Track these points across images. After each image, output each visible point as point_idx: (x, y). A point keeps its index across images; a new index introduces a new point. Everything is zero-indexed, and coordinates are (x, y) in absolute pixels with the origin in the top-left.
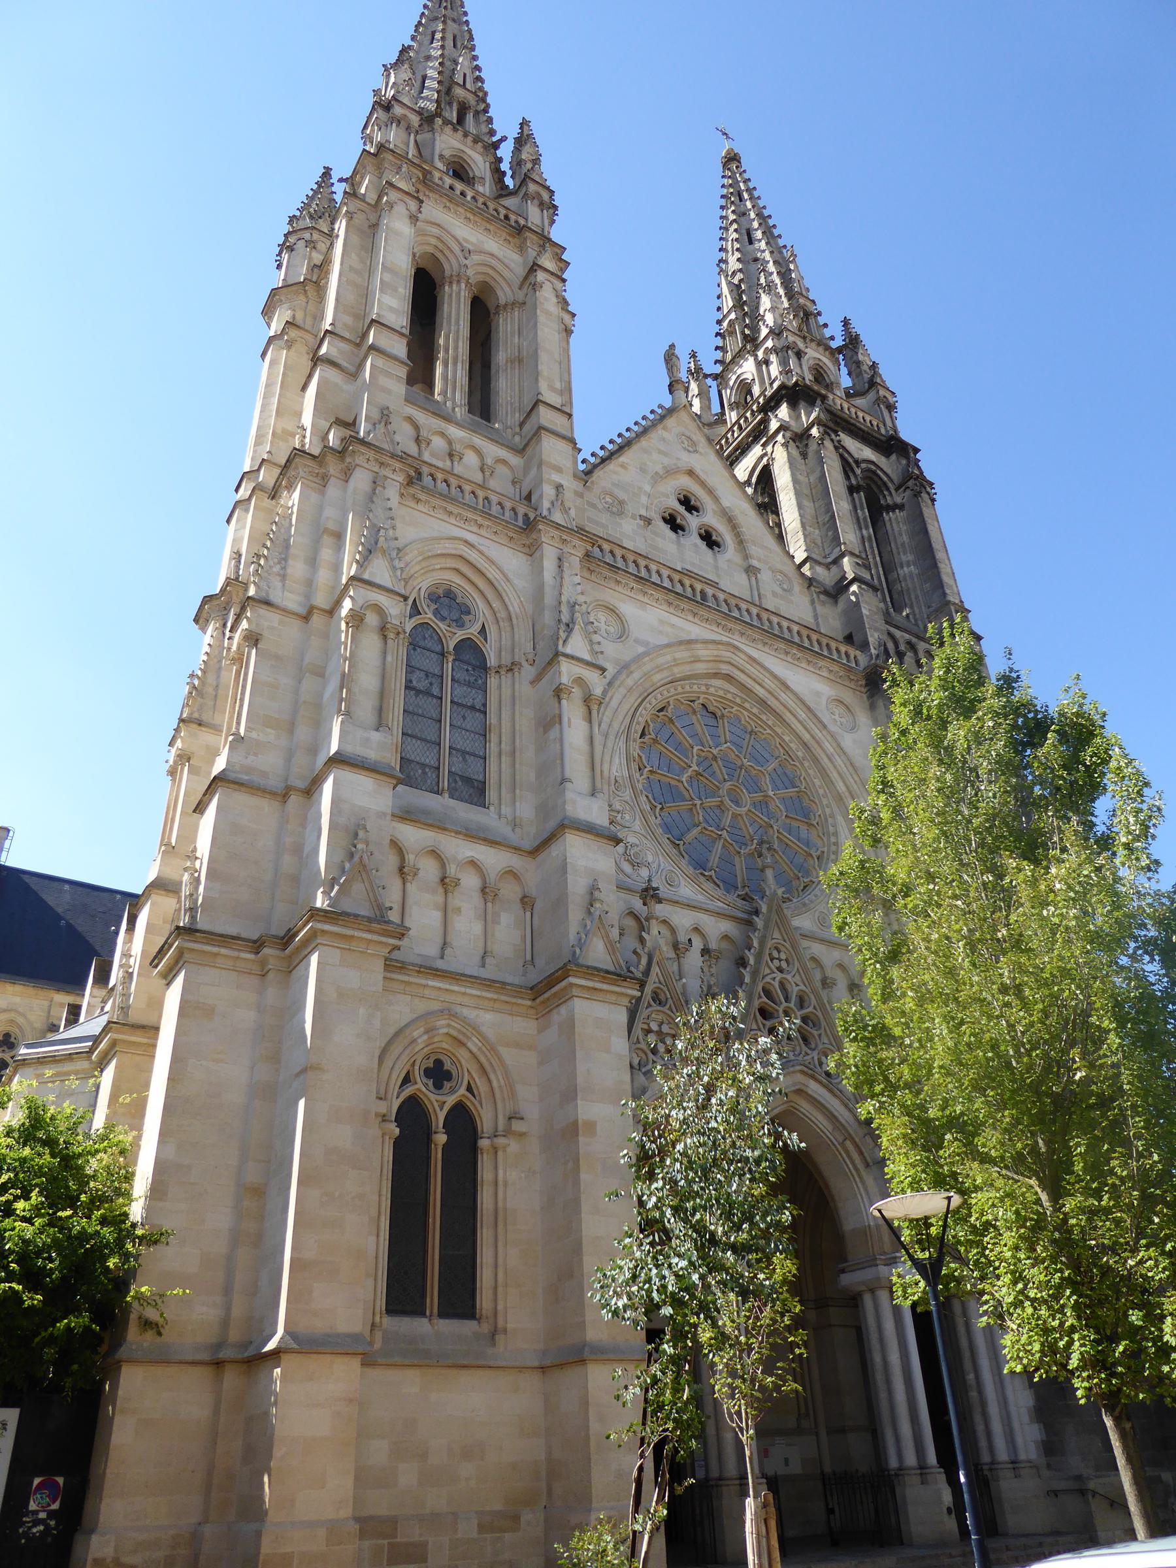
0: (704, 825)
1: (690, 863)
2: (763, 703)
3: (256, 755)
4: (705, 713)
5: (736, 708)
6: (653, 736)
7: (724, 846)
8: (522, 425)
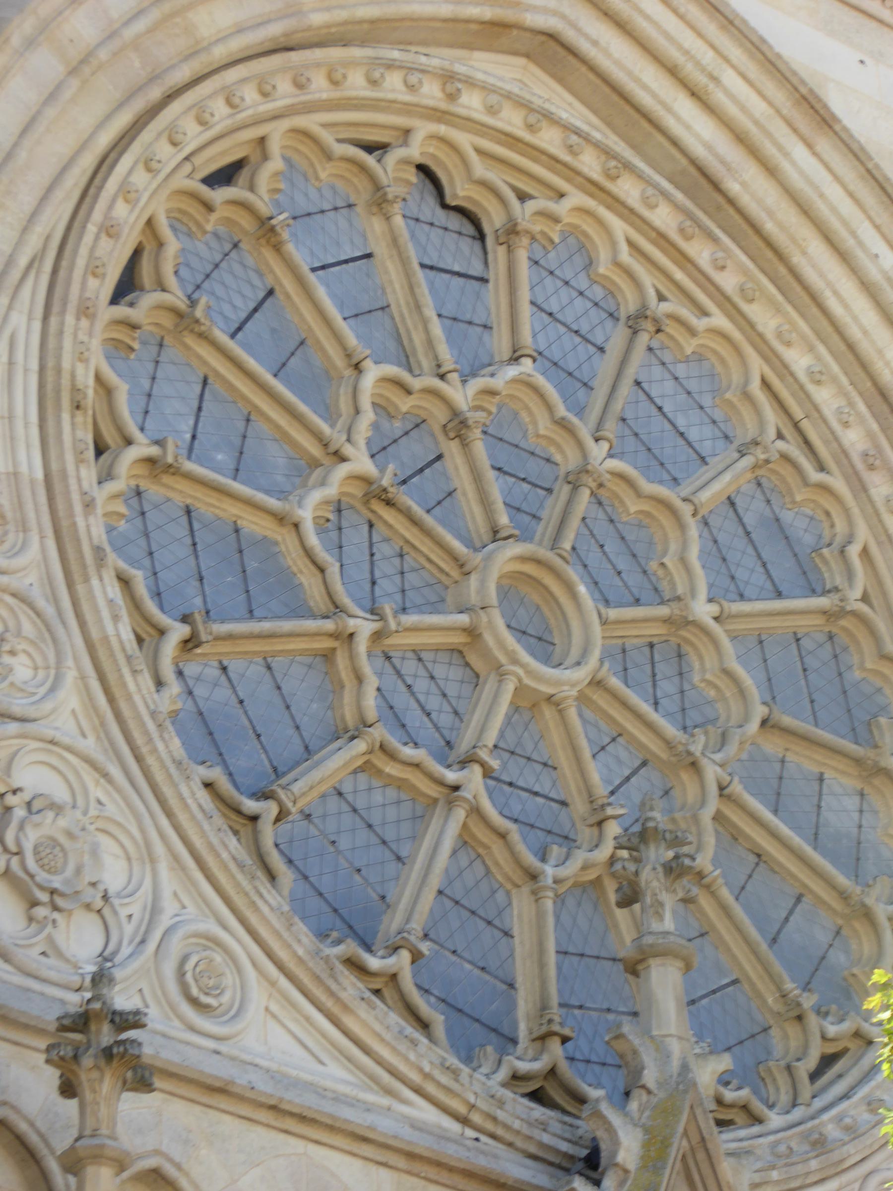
0: (379, 733)
1: (298, 906)
4: (430, 209)
5: (576, 198)
6: (176, 297)
7: (465, 841)
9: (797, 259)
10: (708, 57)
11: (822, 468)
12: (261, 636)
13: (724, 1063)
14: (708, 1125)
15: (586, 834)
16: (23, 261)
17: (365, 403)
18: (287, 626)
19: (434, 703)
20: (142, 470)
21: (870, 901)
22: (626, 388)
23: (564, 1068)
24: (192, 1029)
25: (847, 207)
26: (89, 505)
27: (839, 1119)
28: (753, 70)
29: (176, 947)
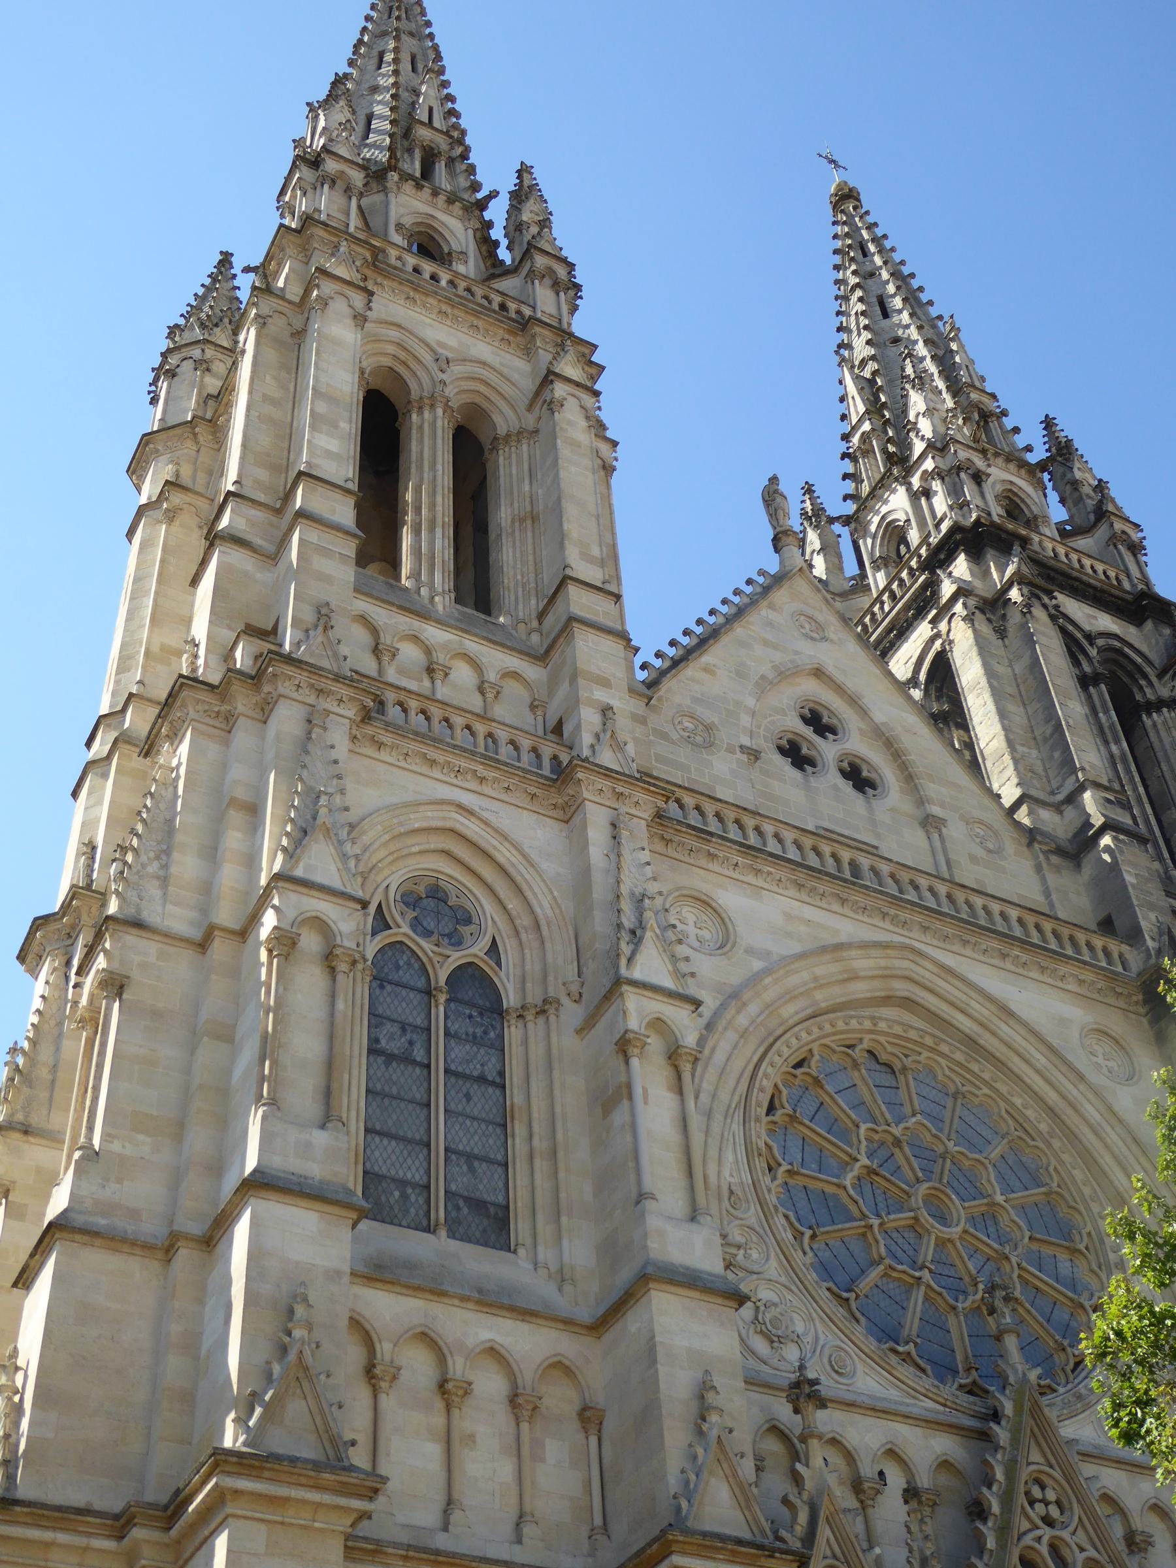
1: (869, 1331)
2: (970, 1042)
3: (119, 1181)
5: (926, 1054)
7: (927, 1298)
8: (541, 616)
9: (1010, 1065)
10: (964, 998)
11: (1033, 1139)
12: (838, 1230)
13: (1039, 1371)
14: (1036, 1395)
15: (971, 1289)
16: (733, 1106)
17: (862, 1138)
18: (847, 1225)
19: (906, 1247)
20: (786, 1175)
21: (1082, 1301)
22: (956, 1120)
23: (979, 1380)
24: (837, 1382)
25: (1024, 1043)
26: (769, 1190)
27: (1086, 1386)
28: (981, 1000)
29: (827, 1352)
